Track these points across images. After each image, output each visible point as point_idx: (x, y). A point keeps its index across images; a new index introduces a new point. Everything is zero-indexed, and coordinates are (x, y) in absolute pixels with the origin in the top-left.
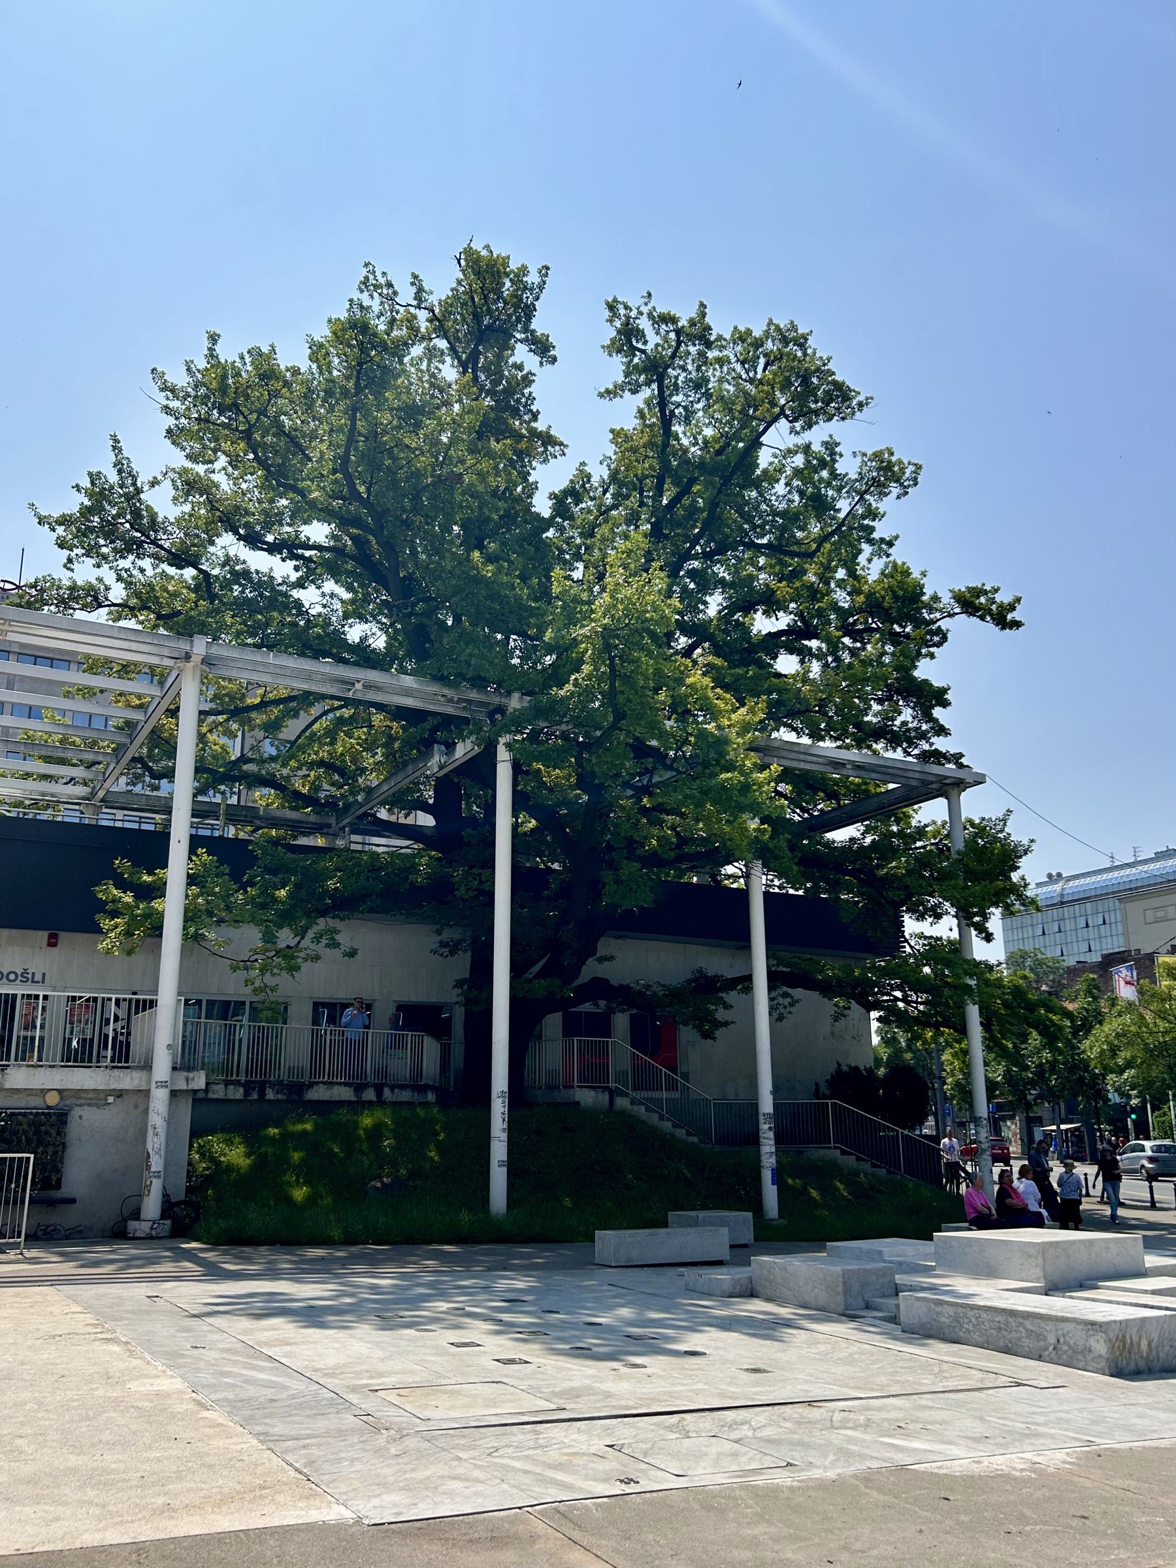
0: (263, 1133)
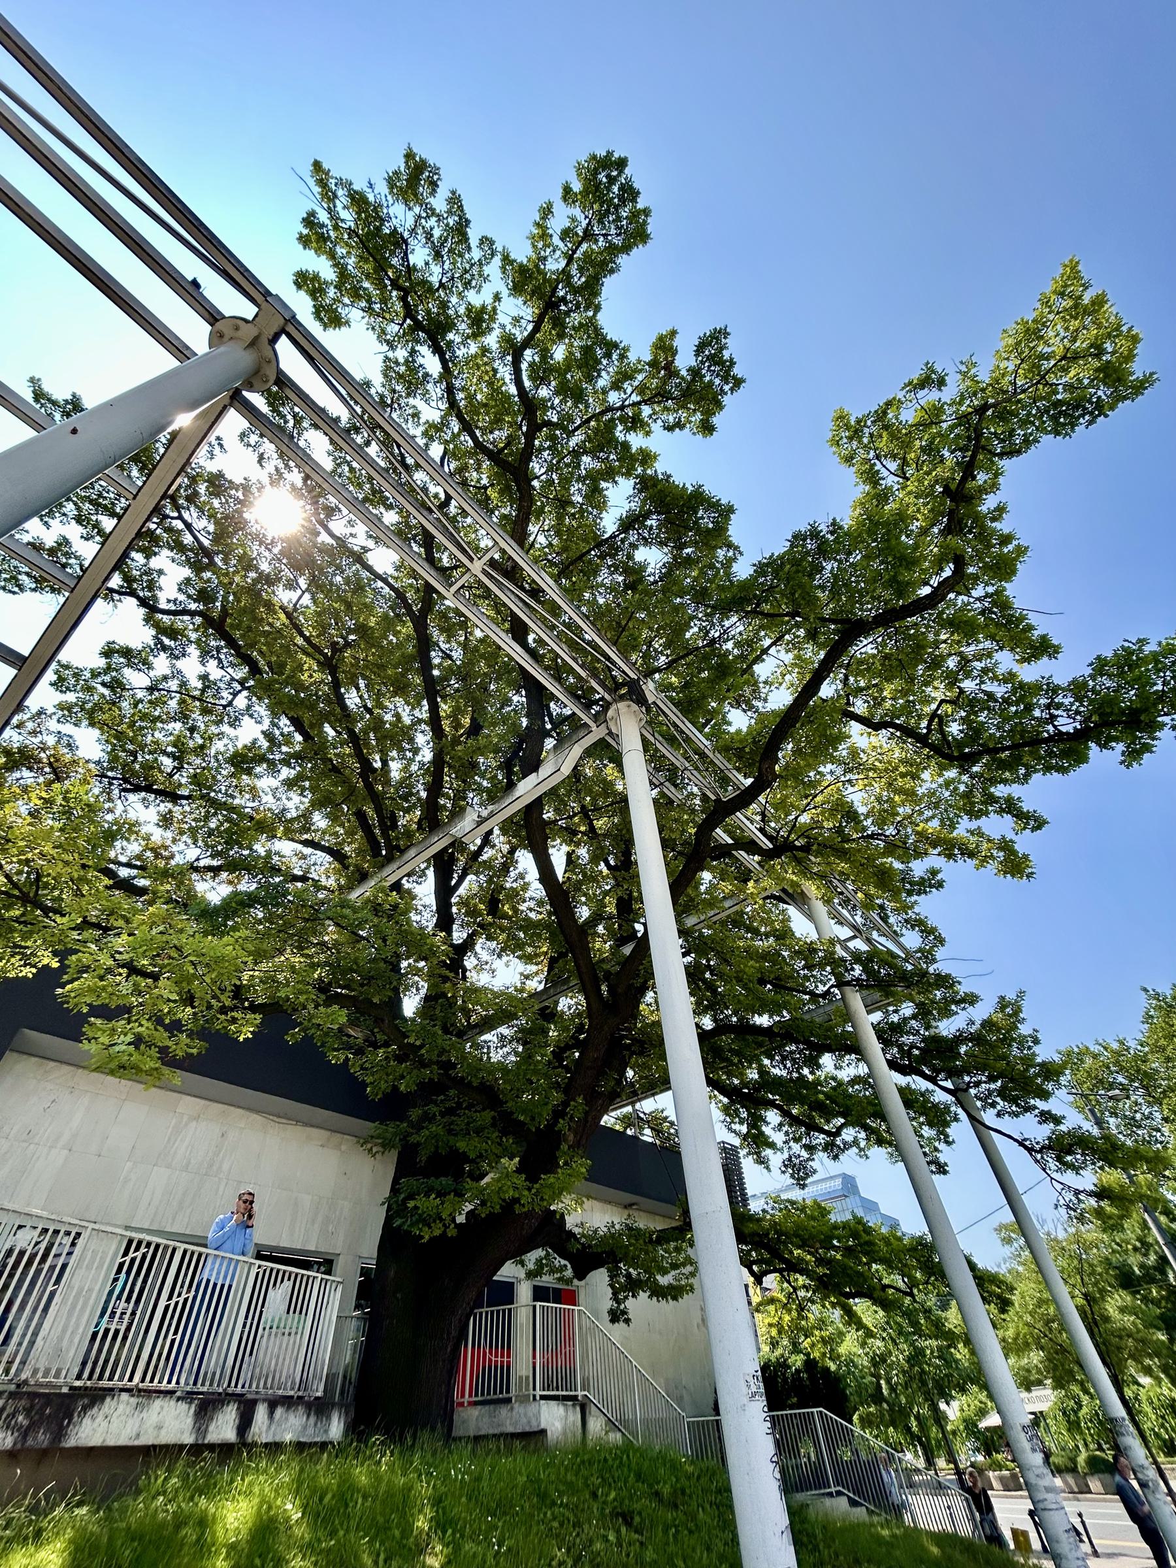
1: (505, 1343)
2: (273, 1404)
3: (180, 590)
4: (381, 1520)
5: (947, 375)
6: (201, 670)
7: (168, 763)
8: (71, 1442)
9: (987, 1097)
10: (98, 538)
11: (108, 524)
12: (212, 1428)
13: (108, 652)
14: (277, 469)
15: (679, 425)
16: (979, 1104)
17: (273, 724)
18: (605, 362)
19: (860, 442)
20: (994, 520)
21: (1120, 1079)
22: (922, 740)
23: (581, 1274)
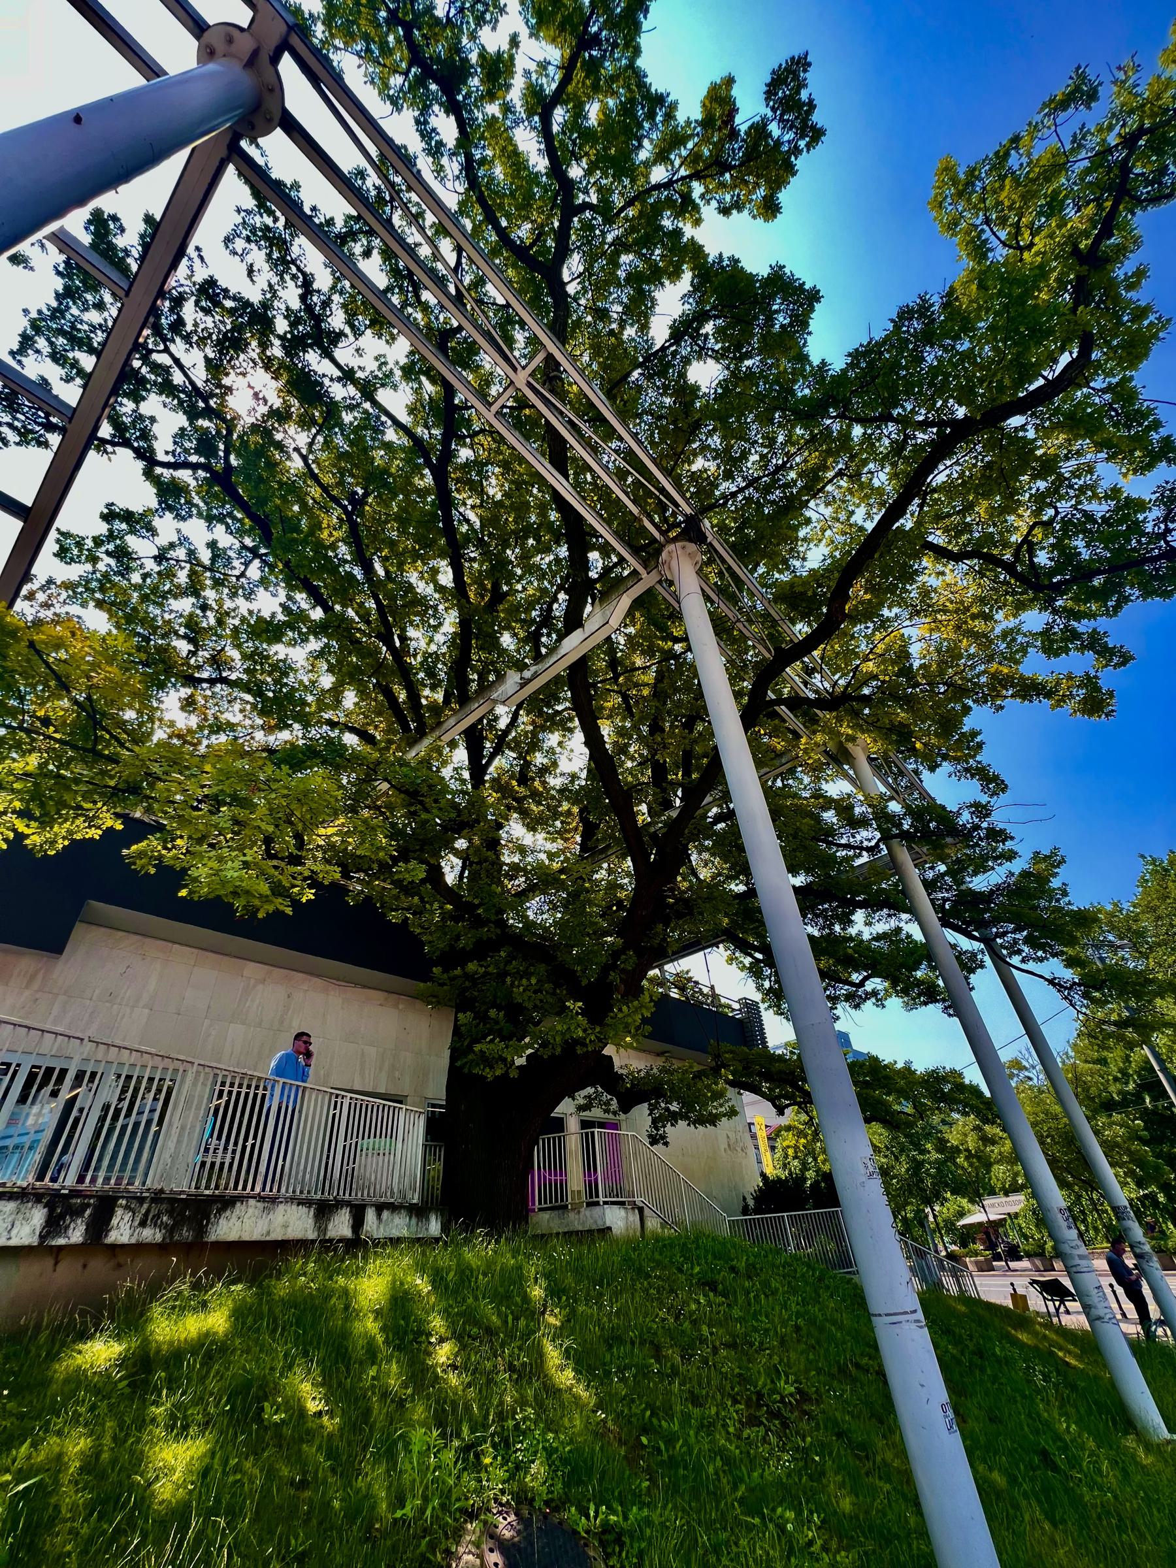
0: (64, 1366)
1: (558, 1164)
2: (380, 1208)
3: (175, 443)
4: (501, 1290)
5: (1100, 84)
6: (209, 537)
7: (183, 647)
8: (212, 1238)
9: (1012, 946)
10: (79, 381)
11: (88, 362)
12: (330, 1226)
13: (109, 516)
14: (270, 285)
15: (738, 206)
16: (1005, 952)
17: (289, 598)
18: (646, 125)
19: (969, 200)
20: (1130, 288)
21: (1111, 938)
22: (1009, 568)
23: (625, 1108)
